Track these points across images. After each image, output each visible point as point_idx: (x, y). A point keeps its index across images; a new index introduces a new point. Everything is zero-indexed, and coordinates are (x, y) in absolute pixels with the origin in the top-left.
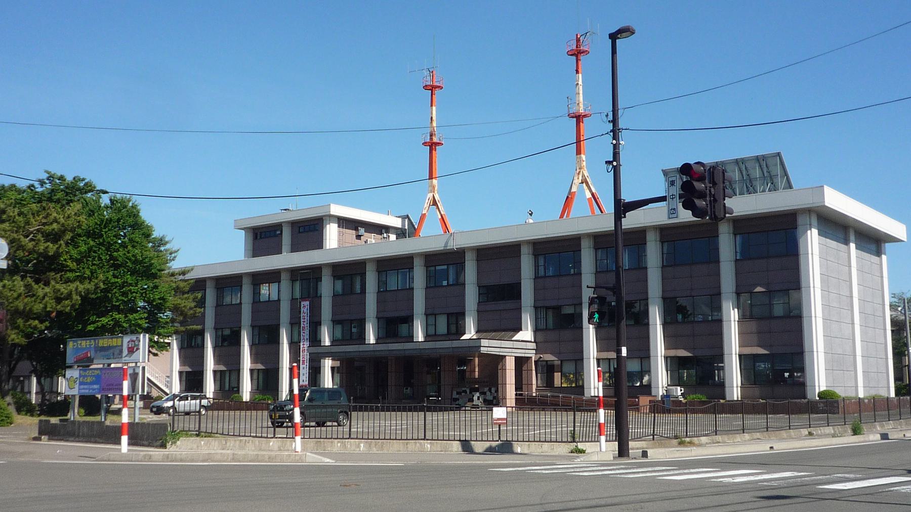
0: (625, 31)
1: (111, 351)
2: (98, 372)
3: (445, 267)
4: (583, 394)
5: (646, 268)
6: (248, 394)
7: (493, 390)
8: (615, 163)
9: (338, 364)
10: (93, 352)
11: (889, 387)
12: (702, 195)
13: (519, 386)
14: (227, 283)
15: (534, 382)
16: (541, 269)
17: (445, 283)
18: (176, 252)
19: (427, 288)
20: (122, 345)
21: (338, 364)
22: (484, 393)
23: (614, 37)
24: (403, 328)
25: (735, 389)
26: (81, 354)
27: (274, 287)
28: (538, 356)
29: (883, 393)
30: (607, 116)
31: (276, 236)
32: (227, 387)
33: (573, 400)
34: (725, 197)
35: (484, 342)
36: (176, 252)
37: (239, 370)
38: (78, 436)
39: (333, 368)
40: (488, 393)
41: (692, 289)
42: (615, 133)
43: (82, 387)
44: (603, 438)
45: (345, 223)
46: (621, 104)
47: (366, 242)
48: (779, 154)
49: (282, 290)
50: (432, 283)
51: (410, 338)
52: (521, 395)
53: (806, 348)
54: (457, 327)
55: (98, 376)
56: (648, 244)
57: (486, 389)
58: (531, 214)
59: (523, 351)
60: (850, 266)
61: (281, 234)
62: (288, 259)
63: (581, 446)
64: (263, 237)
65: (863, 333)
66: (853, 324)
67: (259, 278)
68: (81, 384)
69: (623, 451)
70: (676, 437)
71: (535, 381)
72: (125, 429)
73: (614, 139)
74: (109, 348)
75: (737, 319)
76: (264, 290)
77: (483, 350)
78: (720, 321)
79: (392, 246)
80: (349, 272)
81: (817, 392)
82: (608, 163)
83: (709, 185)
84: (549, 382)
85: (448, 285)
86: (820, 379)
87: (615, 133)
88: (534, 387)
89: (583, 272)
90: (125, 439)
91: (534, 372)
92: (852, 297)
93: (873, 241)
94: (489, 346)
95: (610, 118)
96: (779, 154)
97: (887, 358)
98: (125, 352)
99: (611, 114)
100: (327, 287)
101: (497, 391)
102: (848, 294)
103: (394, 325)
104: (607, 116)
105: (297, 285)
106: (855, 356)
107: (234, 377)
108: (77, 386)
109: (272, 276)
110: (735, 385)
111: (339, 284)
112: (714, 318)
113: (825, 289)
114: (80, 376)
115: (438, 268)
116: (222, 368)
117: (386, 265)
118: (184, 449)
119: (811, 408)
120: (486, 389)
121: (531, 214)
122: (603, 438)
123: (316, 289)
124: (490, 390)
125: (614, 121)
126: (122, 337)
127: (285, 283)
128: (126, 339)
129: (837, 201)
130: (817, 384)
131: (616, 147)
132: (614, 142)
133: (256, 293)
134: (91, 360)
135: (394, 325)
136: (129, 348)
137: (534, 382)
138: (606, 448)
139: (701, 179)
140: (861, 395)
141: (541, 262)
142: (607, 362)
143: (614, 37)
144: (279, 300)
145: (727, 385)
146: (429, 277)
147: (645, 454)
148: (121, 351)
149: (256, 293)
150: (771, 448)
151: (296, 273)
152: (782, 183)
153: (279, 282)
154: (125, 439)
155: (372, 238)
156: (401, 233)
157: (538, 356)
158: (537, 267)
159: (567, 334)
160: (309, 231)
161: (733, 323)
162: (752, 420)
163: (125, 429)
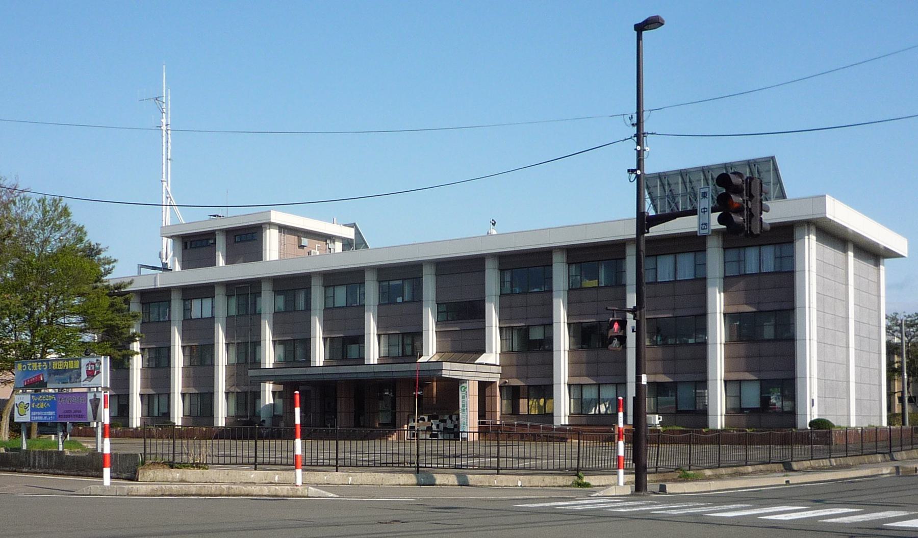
0: (653, 23)
1: (67, 374)
2: (53, 397)
3: (400, 282)
4: (553, 423)
5: (625, 285)
6: (180, 420)
7: (454, 418)
8: (639, 172)
9: (280, 388)
10: (46, 376)
11: (881, 416)
12: (739, 211)
13: (482, 414)
14: (155, 299)
15: (498, 409)
16: (508, 285)
17: (399, 300)
18: (115, 261)
19: (380, 305)
20: (80, 368)
21: (280, 388)
22: (445, 421)
23: (640, 28)
24: (353, 350)
25: (719, 417)
26: (32, 378)
27: (207, 303)
28: (504, 380)
29: (875, 423)
30: (631, 118)
31: (208, 245)
32: (156, 414)
33: (542, 429)
34: (762, 210)
35: (446, 365)
36: (115, 261)
37: (169, 395)
38: (34, 467)
39: (274, 393)
40: (449, 421)
41: (674, 309)
42: (639, 137)
43: (34, 413)
44: (621, 471)
45: (284, 229)
46: (646, 106)
47: (309, 253)
48: (773, 158)
49: (216, 305)
50: (387, 299)
51: (361, 360)
52: (483, 423)
53: (799, 374)
54: (413, 348)
55: (53, 403)
56: (628, 258)
57: (446, 417)
58: (494, 224)
59: (488, 375)
60: (847, 285)
61: (215, 243)
62: (222, 270)
63: (586, 479)
64: (195, 246)
65: (858, 357)
66: (848, 347)
67: (191, 293)
68: (32, 410)
69: (639, 486)
70: (679, 469)
71: (499, 405)
72: (108, 460)
73: (638, 143)
74: (65, 371)
75: (723, 341)
76: (196, 304)
77: (445, 374)
78: (705, 344)
79: (337, 258)
80: (292, 286)
81: (808, 421)
82: (631, 171)
83: (745, 198)
84: (514, 409)
85: (403, 302)
86: (812, 408)
87: (639, 137)
88: (499, 414)
89: (555, 288)
90: (107, 472)
91: (498, 399)
92: (847, 318)
93: (872, 253)
94: (450, 370)
95: (635, 120)
96: (773, 158)
97: (880, 385)
98: (84, 375)
99: (635, 116)
100: (267, 302)
101: (458, 419)
102: (843, 315)
103: (347, 344)
104: (631, 118)
105: (233, 301)
106: (848, 382)
107: (163, 399)
108: (28, 413)
109: (205, 291)
110: (719, 413)
111: (281, 300)
112: (699, 340)
113: (821, 310)
114: (32, 401)
115: (391, 283)
116: (151, 392)
117: (332, 278)
118: (154, 481)
119: (804, 438)
120: (446, 417)
121: (494, 224)
122: (621, 471)
123: (255, 304)
124: (451, 418)
125: (639, 124)
126: (80, 360)
127: (220, 299)
128: (85, 361)
129: (839, 212)
130: (808, 413)
131: (639, 154)
132: (639, 148)
133: (187, 310)
134: (44, 385)
135: (347, 344)
136: (88, 372)
137: (498, 409)
138: (623, 480)
139: (738, 190)
140: (853, 424)
141: (508, 277)
142: (579, 388)
143: (640, 28)
144: (213, 317)
145: (710, 412)
146: (382, 293)
147: (663, 489)
148: (79, 375)
149: (187, 310)
150: (787, 482)
151: (234, 288)
152: (774, 189)
153: (213, 297)
154: (107, 472)
155: (316, 248)
156: (348, 244)
157: (504, 380)
158: (502, 283)
159: (535, 357)
160: (246, 239)
161: (719, 346)
162: (733, 453)
163: (108, 460)
